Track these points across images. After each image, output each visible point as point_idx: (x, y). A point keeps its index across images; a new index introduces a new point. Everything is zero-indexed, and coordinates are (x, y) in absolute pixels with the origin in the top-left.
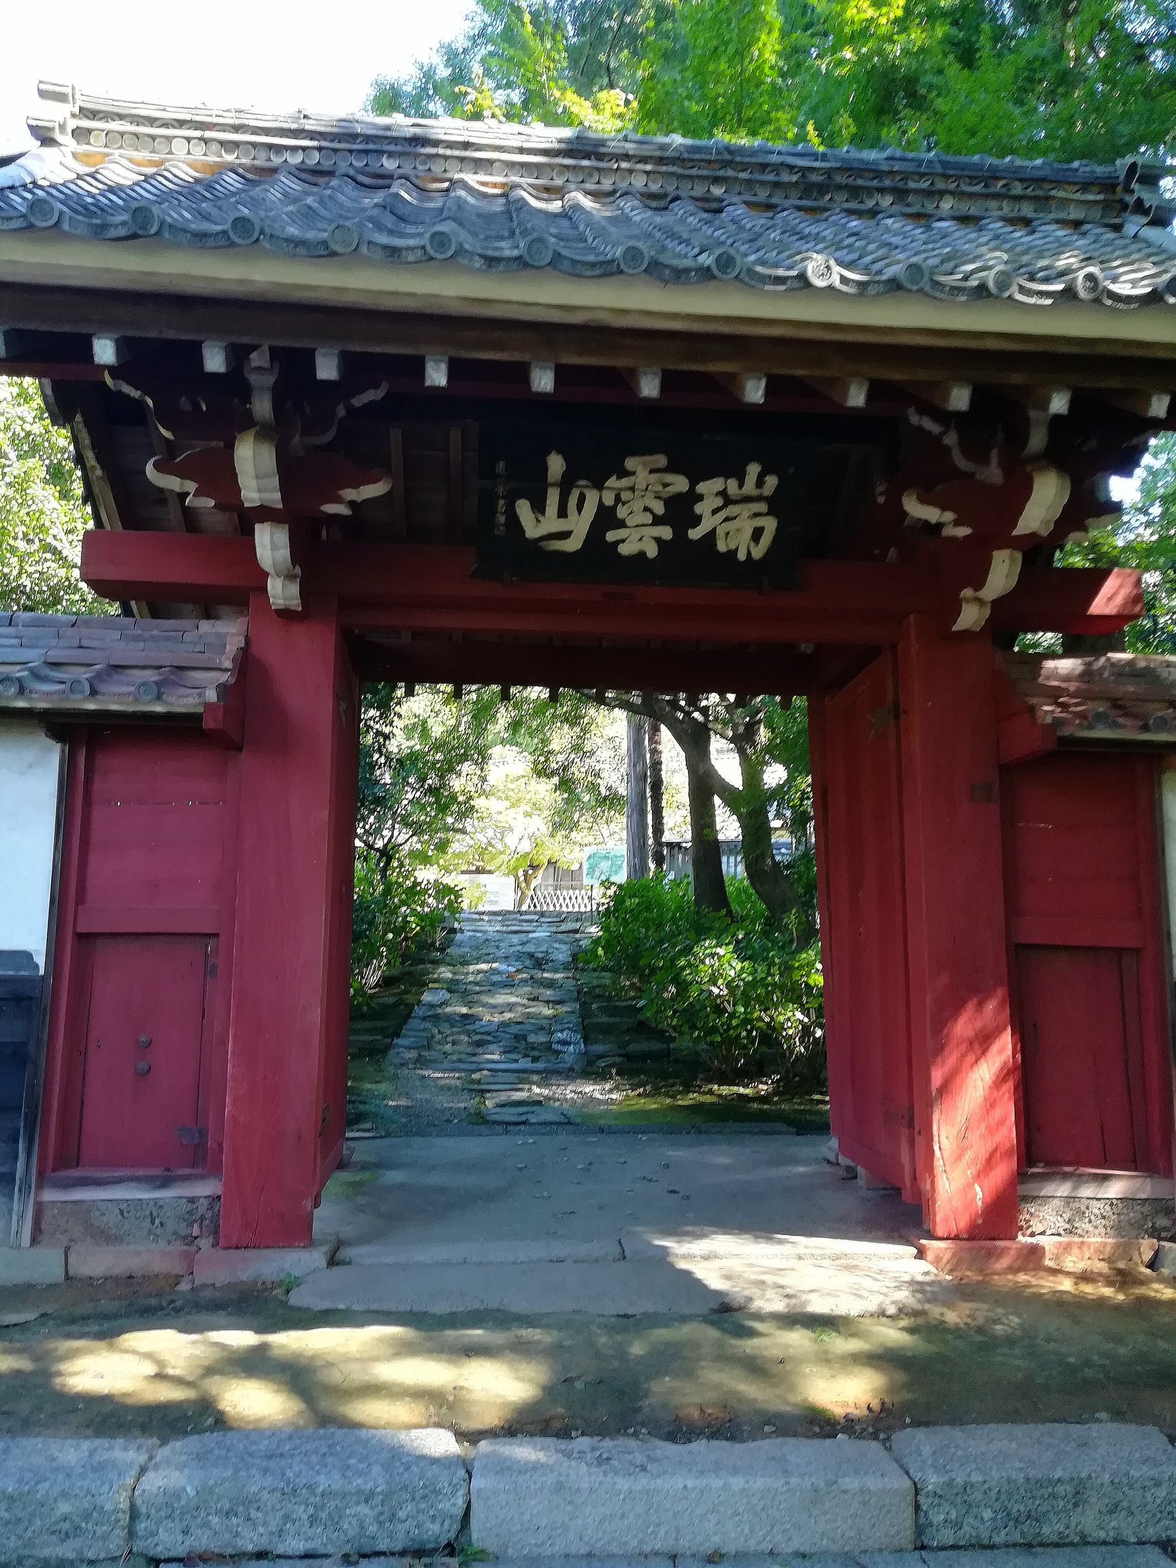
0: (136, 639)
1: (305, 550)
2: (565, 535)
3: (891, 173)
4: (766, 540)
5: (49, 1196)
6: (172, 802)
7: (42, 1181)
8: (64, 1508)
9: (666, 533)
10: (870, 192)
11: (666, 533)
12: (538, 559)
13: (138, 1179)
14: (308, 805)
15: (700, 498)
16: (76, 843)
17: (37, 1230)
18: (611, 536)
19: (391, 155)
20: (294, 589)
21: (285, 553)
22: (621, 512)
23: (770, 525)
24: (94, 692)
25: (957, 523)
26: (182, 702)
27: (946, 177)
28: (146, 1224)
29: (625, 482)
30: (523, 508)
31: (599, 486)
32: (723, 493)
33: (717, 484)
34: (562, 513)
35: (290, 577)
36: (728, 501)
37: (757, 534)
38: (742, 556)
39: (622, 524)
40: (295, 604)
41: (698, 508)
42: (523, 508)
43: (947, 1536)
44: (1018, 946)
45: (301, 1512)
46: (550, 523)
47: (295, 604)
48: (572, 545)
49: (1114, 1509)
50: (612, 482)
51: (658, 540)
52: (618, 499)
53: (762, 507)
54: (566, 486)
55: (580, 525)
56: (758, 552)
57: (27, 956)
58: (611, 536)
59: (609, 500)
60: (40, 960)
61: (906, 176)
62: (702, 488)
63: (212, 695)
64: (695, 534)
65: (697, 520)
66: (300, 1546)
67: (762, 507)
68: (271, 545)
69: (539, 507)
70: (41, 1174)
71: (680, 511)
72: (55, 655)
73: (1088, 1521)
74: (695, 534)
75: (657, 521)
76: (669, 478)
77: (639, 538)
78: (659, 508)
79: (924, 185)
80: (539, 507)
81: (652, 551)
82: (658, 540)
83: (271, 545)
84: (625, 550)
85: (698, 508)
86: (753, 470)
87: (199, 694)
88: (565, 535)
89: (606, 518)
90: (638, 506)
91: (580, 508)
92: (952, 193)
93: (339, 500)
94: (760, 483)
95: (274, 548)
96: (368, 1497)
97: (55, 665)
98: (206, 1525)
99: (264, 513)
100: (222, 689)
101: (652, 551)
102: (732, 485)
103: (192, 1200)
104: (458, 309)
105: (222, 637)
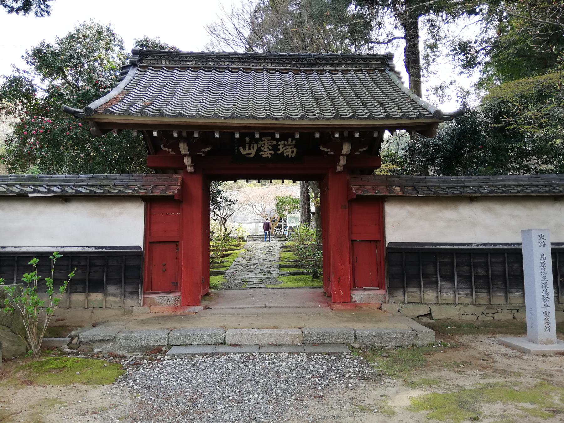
0: (160, 179)
1: (195, 160)
2: (251, 154)
3: (330, 59)
4: (294, 153)
5: (146, 296)
6: (168, 214)
7: (145, 293)
8: (157, 337)
9: (273, 152)
10: (324, 64)
11: (273, 152)
12: (245, 159)
13: (164, 292)
14: (197, 214)
15: (279, 145)
16: (148, 222)
17: (144, 303)
18: (260, 153)
19: (212, 62)
20: (192, 168)
21: (190, 162)
22: (262, 149)
23: (295, 150)
24: (152, 192)
25: (331, 152)
26: (170, 193)
27: (343, 59)
28: (166, 302)
29: (262, 143)
30: (241, 149)
31: (257, 144)
32: (284, 144)
33: (283, 142)
34: (249, 149)
35: (191, 166)
36: (285, 146)
37: (292, 152)
38: (290, 156)
39: (263, 151)
40: (193, 171)
41: (279, 147)
42: (241, 149)
43: (308, 342)
44: (352, 241)
45: (196, 338)
46: (247, 151)
47: (193, 171)
48: (252, 155)
49: (338, 338)
50: (260, 142)
51: (271, 154)
52: (261, 146)
53: (293, 146)
54: (250, 144)
55: (254, 151)
56: (293, 156)
57: (139, 247)
58: (260, 153)
59: (259, 146)
60: (142, 248)
61: (333, 60)
62: (279, 143)
63: (176, 192)
64: (279, 152)
65: (279, 150)
66: (196, 343)
67: (293, 146)
68: (187, 161)
69: (244, 148)
70: (144, 292)
71: (275, 148)
72: (143, 183)
73: (333, 340)
74: (279, 152)
75: (270, 150)
76: (272, 141)
77: (267, 154)
78: (270, 147)
79: (337, 62)
80: (244, 148)
81: (270, 156)
82: (271, 154)
83: (187, 161)
84: (264, 156)
85: (279, 147)
86: (290, 139)
87: (174, 191)
88: (251, 154)
89: (259, 150)
90: (266, 147)
91: (253, 148)
92: (345, 64)
93: (201, 152)
94: (292, 142)
95: (188, 161)
96: (208, 335)
97: (143, 185)
98: (181, 340)
99: (185, 155)
100: (178, 190)
101: (270, 156)
102: (286, 143)
103: (175, 296)
104: (220, 125)
105: (178, 178)
